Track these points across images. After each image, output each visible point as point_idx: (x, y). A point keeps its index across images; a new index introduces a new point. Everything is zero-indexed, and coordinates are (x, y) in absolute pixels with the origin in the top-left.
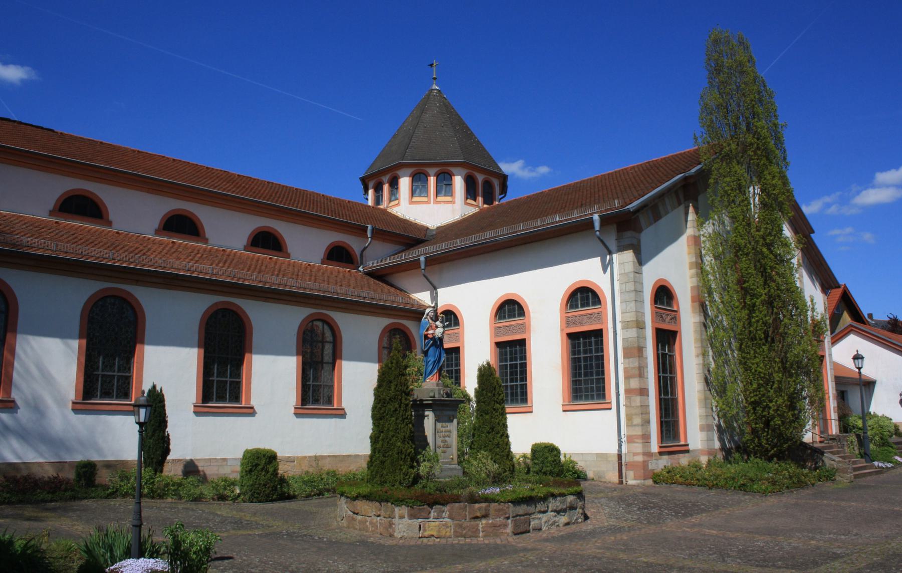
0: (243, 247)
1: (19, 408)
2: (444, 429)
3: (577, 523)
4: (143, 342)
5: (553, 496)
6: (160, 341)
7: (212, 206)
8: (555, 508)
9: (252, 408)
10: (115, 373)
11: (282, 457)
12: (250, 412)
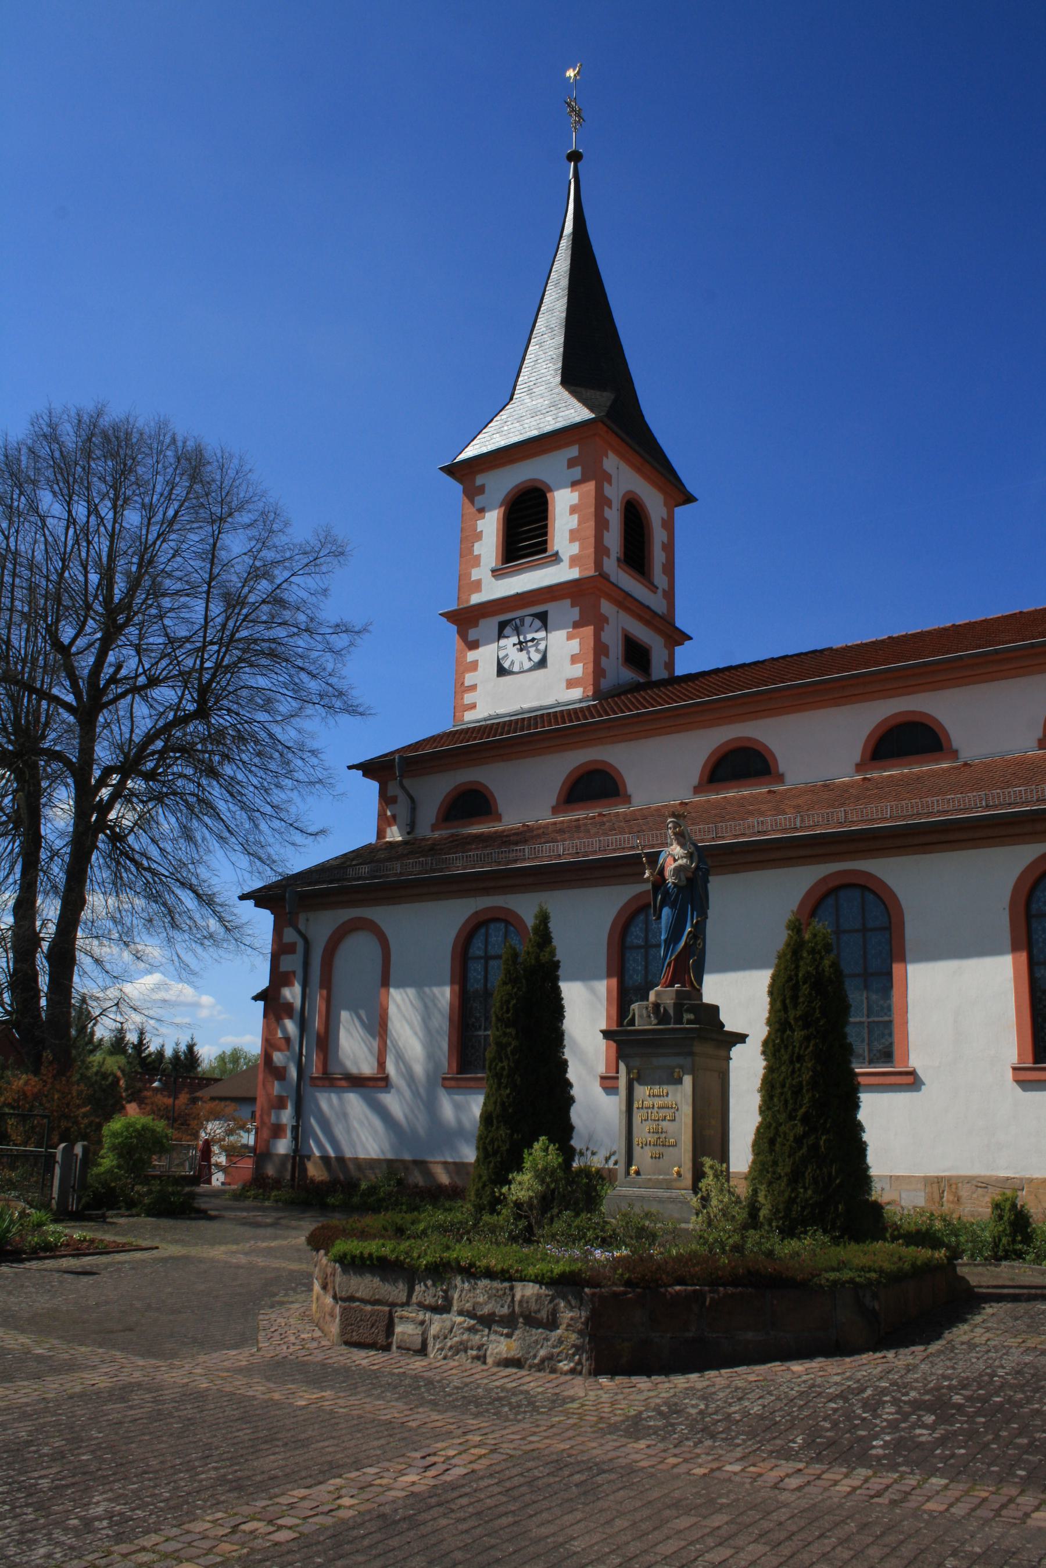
0: (1035, 744)
1: (924, 1084)
2: (658, 1102)
3: (553, 1371)
4: (903, 959)
5: (470, 1272)
6: (933, 954)
7: (885, 698)
8: (468, 1306)
9: (913, 1073)
10: (864, 1019)
11: (990, 1177)
12: (911, 1081)
